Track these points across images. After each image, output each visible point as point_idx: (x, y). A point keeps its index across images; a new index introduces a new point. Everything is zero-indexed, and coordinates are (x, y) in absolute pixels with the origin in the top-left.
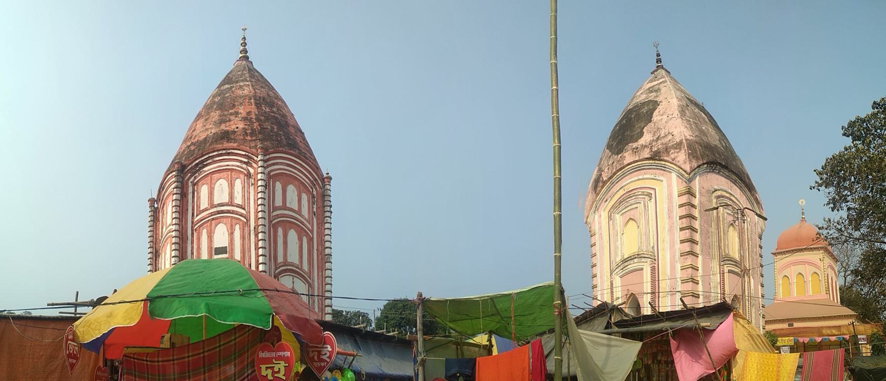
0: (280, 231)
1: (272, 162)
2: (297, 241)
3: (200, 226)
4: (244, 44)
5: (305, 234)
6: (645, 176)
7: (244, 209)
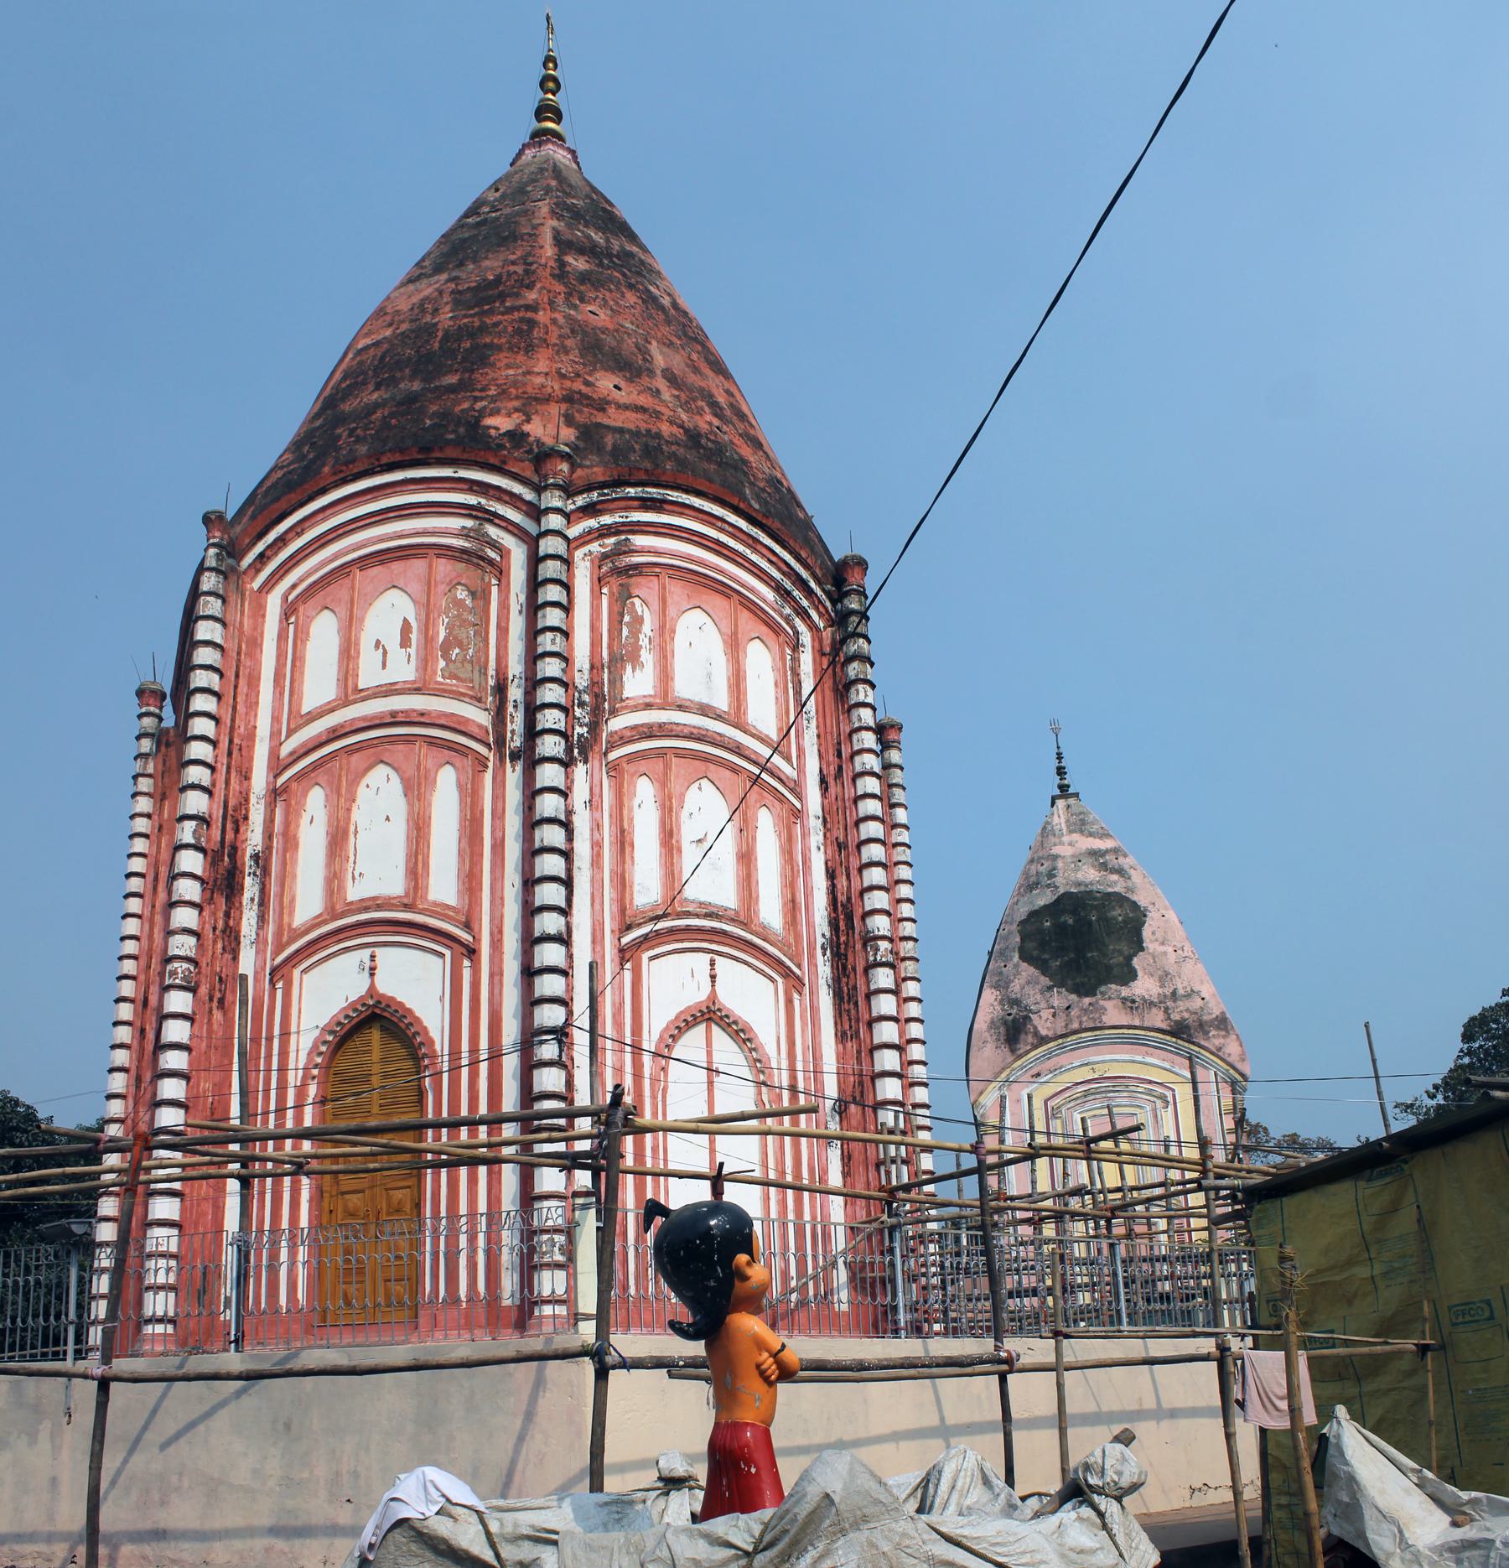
6: (1149, 1060)
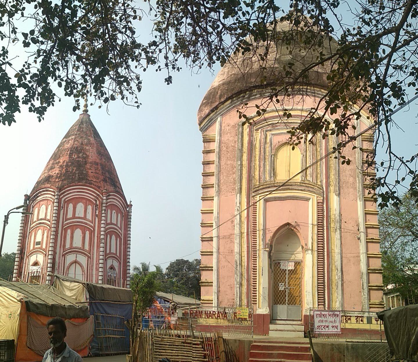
0: (69, 231)
1: (67, 193)
2: (82, 234)
3: (32, 231)
7: (50, 222)
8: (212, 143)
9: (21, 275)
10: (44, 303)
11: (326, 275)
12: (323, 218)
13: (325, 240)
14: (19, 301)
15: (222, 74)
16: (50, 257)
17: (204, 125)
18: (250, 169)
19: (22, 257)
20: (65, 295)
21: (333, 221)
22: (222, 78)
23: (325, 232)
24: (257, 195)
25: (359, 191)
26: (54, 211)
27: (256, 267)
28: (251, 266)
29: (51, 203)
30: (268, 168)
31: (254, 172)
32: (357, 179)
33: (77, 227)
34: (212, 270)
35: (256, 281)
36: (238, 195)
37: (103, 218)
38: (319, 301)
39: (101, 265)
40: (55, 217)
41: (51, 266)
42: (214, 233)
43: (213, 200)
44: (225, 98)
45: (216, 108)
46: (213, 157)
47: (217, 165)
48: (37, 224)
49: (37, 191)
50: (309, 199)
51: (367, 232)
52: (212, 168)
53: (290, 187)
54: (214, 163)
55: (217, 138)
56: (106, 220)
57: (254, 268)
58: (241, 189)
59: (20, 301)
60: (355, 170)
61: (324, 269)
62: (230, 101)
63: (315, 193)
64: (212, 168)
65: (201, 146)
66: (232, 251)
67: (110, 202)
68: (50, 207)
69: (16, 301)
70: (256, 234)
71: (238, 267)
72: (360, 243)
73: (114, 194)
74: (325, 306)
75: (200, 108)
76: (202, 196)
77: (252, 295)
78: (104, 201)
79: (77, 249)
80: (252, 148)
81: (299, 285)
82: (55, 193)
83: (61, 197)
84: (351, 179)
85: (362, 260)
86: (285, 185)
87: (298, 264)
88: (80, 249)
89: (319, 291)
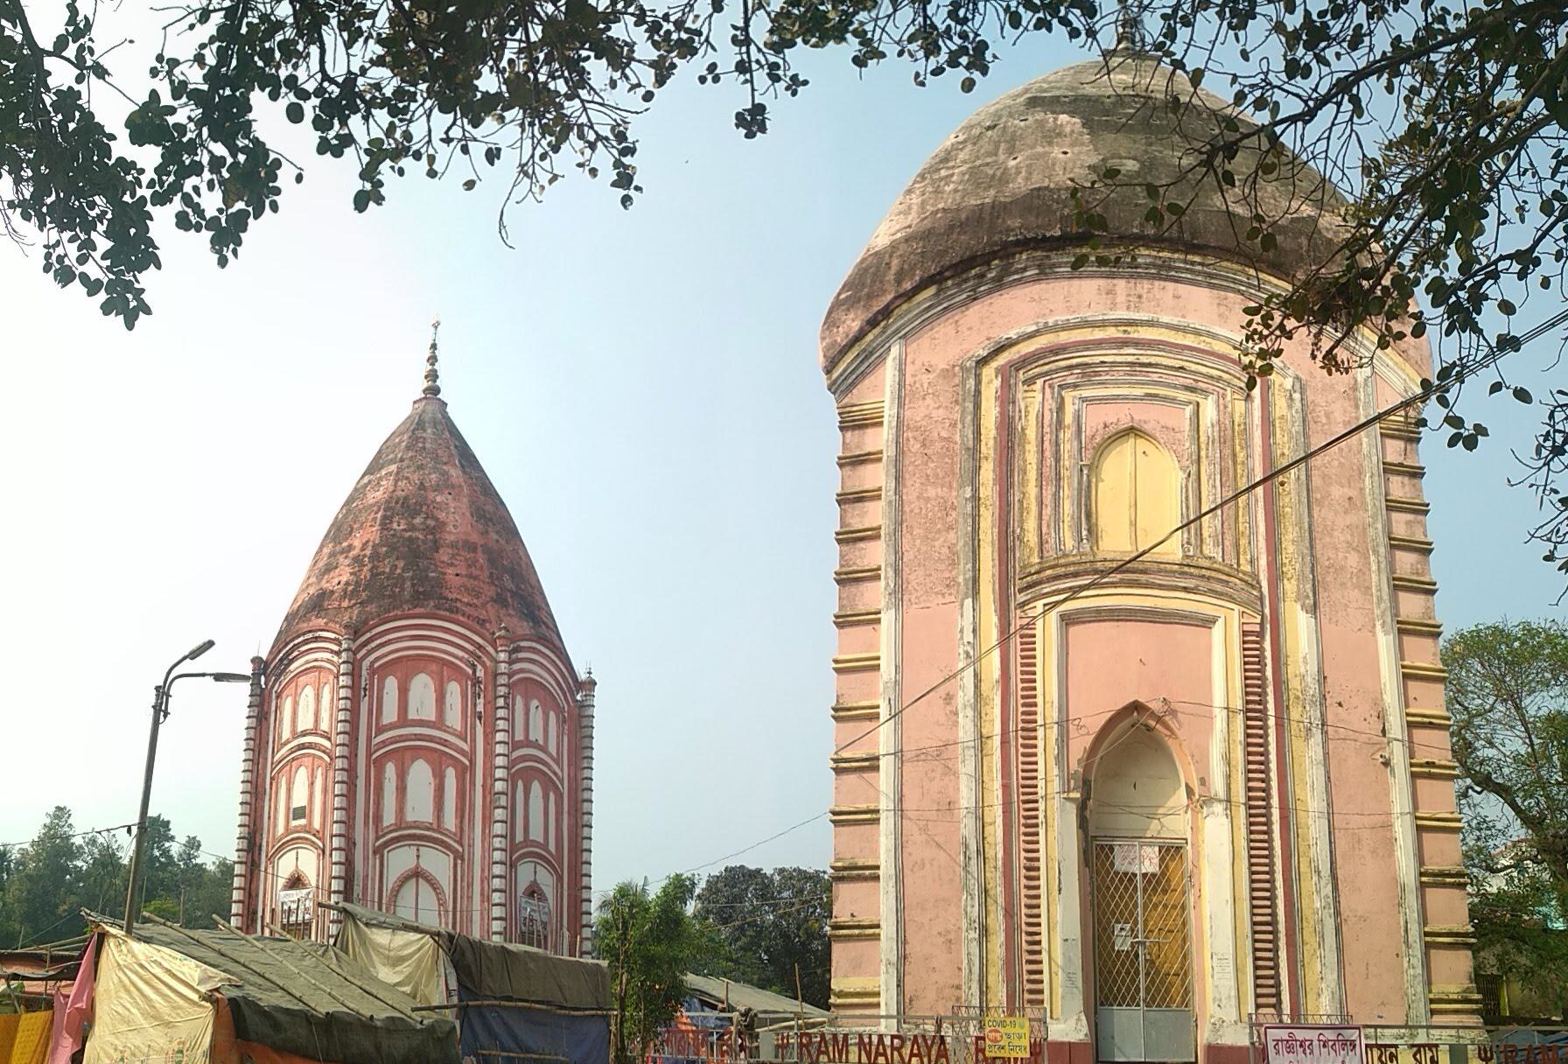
0: (390, 770)
1: (378, 642)
2: (432, 779)
4: (433, 359)
5: (450, 761)
8: (870, 431)
9: (254, 921)
10: (300, 1006)
11: (1280, 892)
12: (1263, 686)
13: (1273, 766)
14: (204, 999)
15: (900, 213)
16: (336, 856)
17: (844, 371)
18: (1009, 512)
19: (253, 860)
20: (375, 979)
21: (1298, 698)
22: (904, 221)
23: (1272, 739)
24: (1034, 599)
25: (1380, 599)
26: (342, 704)
27: (1038, 859)
28: (1020, 859)
29: (331, 677)
30: (1068, 508)
31: (1022, 521)
32: (1372, 558)
33: (417, 752)
34: (877, 878)
35: (1039, 916)
36: (968, 602)
37: (501, 724)
38: (1260, 991)
39: (497, 883)
40: (345, 721)
41: (342, 889)
42: (883, 739)
43: (878, 621)
44: (917, 278)
45: (886, 312)
46: (876, 476)
47: (890, 502)
48: (292, 751)
49: (287, 644)
50: (1214, 621)
51: (1411, 741)
52: (875, 514)
53: (1143, 578)
54: (879, 497)
55: (889, 413)
56: (510, 731)
57: (1028, 864)
58: (975, 581)
59: (208, 997)
60: (1364, 529)
61: (1271, 873)
62: (932, 290)
63: (1232, 599)
64: (875, 514)
65: (834, 443)
66: (951, 806)
67: (522, 671)
68: (326, 692)
69: (195, 997)
70: (1035, 738)
71: (974, 862)
72: (1391, 780)
73: (534, 645)
74: (1280, 1013)
75: (827, 318)
76: (836, 611)
77: (1026, 967)
78: (503, 667)
79: (418, 828)
80: (1013, 443)
81: (1181, 932)
82: (340, 644)
83: (359, 656)
84: (1353, 560)
85: (1400, 841)
86: (1130, 570)
87: (1171, 851)
88: (428, 829)
89: (1259, 954)
